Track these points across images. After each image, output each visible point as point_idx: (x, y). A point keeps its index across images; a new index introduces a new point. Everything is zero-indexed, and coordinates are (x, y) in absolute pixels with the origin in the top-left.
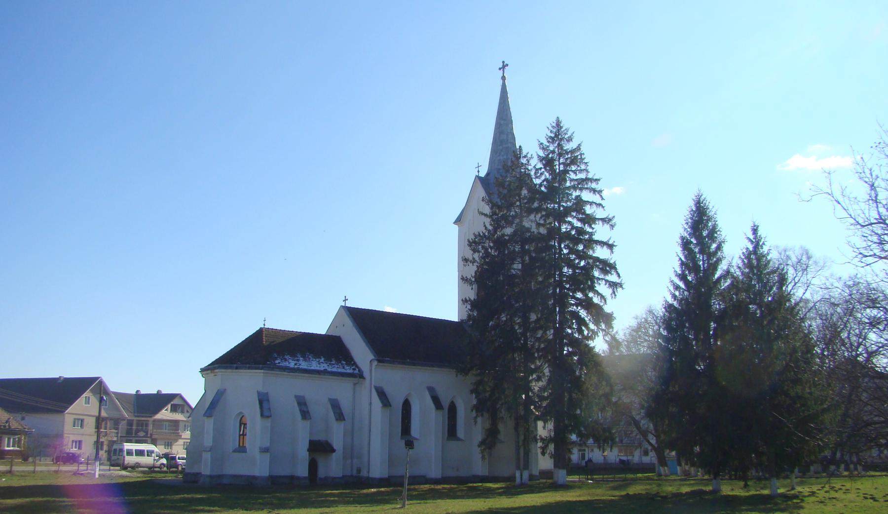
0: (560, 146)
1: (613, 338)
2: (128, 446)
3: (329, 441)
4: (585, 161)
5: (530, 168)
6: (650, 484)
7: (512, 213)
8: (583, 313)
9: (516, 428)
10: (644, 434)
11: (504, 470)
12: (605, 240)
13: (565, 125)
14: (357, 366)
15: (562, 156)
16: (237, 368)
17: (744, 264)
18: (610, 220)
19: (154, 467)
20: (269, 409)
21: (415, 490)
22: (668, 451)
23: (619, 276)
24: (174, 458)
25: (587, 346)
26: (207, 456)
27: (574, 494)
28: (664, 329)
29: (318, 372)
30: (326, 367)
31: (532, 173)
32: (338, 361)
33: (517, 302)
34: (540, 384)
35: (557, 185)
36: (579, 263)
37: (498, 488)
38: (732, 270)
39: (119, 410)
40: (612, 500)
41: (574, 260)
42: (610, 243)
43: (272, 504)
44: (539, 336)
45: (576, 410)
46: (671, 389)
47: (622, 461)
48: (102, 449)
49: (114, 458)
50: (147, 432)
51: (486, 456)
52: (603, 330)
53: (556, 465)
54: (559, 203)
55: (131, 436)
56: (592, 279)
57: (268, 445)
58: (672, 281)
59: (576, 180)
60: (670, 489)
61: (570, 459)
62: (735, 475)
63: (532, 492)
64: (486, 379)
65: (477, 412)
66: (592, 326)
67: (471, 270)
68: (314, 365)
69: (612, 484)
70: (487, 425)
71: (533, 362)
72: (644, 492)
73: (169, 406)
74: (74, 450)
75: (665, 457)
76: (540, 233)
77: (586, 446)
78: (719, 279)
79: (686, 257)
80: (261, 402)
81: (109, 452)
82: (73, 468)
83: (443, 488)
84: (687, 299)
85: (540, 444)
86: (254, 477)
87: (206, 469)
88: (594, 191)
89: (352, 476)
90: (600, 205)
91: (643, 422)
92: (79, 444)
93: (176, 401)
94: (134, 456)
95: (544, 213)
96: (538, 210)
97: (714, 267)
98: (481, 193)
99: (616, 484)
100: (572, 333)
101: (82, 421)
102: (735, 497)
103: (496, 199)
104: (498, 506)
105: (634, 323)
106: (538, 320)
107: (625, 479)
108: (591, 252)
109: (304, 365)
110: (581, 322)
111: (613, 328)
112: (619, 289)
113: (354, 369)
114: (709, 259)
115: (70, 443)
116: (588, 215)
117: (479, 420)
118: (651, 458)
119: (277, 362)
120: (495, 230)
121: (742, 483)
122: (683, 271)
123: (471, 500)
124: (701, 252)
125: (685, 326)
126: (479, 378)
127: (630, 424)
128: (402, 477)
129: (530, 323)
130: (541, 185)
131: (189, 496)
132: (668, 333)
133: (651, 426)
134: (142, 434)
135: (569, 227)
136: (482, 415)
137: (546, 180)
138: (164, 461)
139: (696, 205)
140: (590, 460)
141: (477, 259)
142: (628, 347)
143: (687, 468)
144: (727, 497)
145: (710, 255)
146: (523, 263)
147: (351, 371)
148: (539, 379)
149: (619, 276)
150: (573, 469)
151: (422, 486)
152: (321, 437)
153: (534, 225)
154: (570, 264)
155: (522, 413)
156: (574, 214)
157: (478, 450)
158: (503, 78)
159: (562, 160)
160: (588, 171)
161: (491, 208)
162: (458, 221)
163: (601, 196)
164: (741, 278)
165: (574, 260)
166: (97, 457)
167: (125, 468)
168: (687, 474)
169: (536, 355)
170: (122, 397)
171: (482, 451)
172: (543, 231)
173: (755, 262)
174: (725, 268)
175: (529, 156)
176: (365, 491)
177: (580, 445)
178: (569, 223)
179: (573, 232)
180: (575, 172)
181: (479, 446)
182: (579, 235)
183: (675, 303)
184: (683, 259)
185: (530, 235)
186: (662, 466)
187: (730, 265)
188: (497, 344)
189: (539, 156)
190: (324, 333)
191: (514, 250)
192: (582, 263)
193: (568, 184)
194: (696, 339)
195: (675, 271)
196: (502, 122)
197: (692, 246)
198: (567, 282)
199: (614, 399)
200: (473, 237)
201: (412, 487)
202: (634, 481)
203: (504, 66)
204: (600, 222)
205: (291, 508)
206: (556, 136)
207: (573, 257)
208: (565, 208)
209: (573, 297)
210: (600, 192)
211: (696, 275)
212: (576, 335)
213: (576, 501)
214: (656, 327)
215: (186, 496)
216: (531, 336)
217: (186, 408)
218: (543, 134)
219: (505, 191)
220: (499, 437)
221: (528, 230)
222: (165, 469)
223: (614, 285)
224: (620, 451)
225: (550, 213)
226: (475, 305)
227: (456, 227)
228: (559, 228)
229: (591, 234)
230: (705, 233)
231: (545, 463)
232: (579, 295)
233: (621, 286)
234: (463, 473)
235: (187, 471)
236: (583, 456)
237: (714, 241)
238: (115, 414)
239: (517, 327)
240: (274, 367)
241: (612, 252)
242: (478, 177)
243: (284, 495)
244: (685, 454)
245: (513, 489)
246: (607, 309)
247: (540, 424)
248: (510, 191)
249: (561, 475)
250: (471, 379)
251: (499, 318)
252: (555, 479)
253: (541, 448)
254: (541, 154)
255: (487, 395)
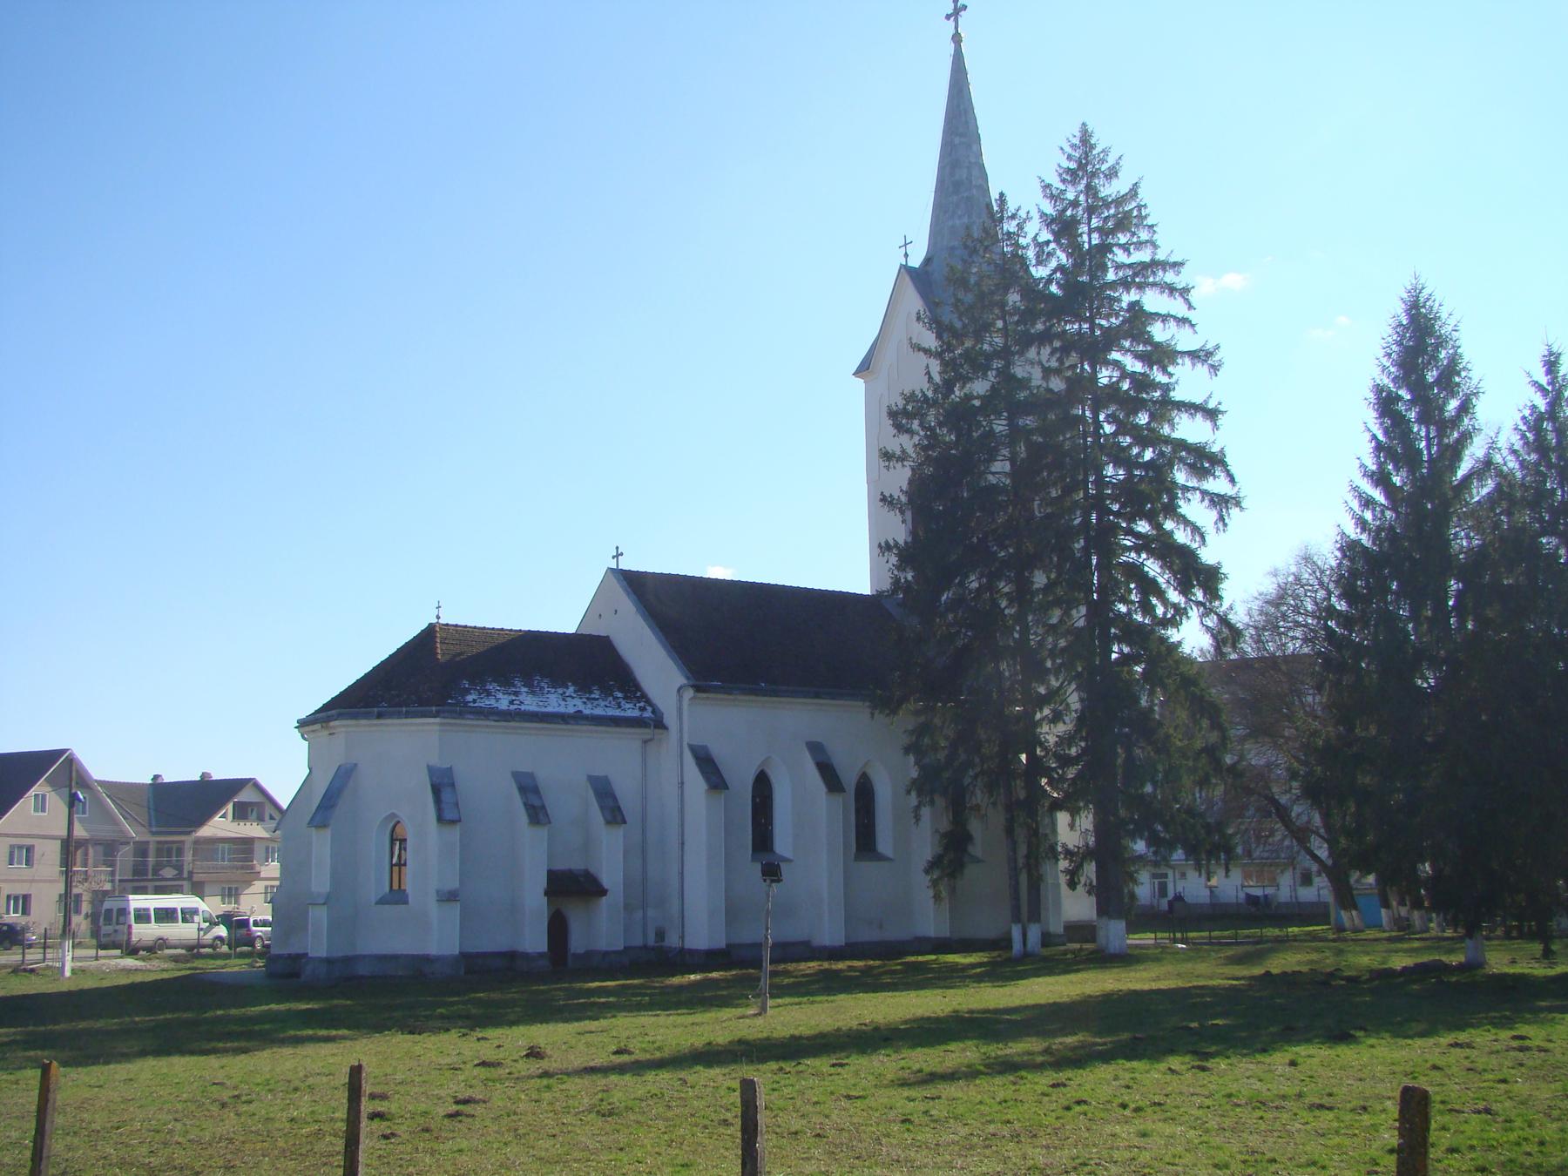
0: (1090, 190)
1: (1224, 620)
2: (137, 902)
3: (592, 870)
4: (1149, 221)
5: (1023, 241)
6: (1317, 950)
8: (1152, 567)
10: (1301, 835)
11: (988, 924)
12: (1198, 401)
13: (1100, 141)
14: (648, 702)
15: (1095, 210)
16: (380, 716)
17: (1527, 443)
18: (1209, 354)
20: (457, 805)
21: (786, 973)
23: (1232, 480)
24: (245, 924)
27: (1145, 974)
28: (1340, 597)
29: (563, 718)
30: (581, 707)
31: (1031, 254)
32: (607, 692)
34: (1061, 728)
35: (1085, 278)
36: (1140, 455)
37: (973, 966)
38: (1498, 459)
39: (115, 822)
40: (1233, 988)
42: (1211, 405)
43: (468, 1017)
44: (1054, 621)
45: (1142, 786)
48: (78, 912)
49: (106, 929)
50: (179, 868)
51: (944, 894)
52: (1199, 604)
53: (1102, 910)
54: (1091, 320)
56: (1171, 489)
57: (453, 883)
58: (1355, 489)
59: (1130, 266)
60: (1365, 960)
61: (1132, 896)
62: (1519, 928)
64: (937, 721)
66: (1174, 596)
67: (899, 479)
68: (554, 702)
69: (1230, 952)
70: (945, 825)
71: (1043, 681)
72: (1305, 969)
73: (230, 806)
76: (1051, 391)
78: (1467, 479)
79: (1386, 432)
80: (437, 790)
81: (94, 917)
83: (851, 968)
84: (1391, 528)
85: (1063, 864)
86: (427, 959)
87: (317, 944)
88: (1171, 289)
89: (645, 947)
90: (1183, 321)
91: (1297, 809)
92: (24, 903)
93: (245, 796)
94: (153, 925)
95: (1057, 344)
96: (1044, 338)
97: (1454, 453)
98: (914, 302)
99: (1240, 950)
100: (1129, 613)
101: (30, 849)
103: (948, 316)
104: (975, 1006)
105: (1270, 587)
108: (1166, 430)
109: (530, 703)
110: (1150, 587)
111: (1220, 598)
112: (1234, 511)
113: (642, 709)
114: (1441, 434)
116: (1157, 346)
117: (926, 812)
118: (1320, 890)
119: (470, 698)
121: (1537, 947)
122: (1380, 465)
123: (913, 994)
124: (1423, 419)
125: (1388, 590)
126: (922, 719)
127: (1269, 814)
128: (758, 946)
129: (1034, 593)
130: (1049, 281)
131: (282, 1007)
132: (1349, 604)
133: (1317, 819)
134: (169, 872)
135: (1116, 374)
136: (932, 803)
137: (1060, 268)
138: (222, 931)
139: (1408, 312)
140: (1179, 898)
141: (910, 451)
142: (1258, 640)
143: (1403, 911)
145: (1444, 425)
146: (1012, 460)
147: (636, 713)
148: (1056, 718)
149: (1232, 480)
150: (1143, 919)
151: (803, 966)
152: (575, 864)
153: (1037, 374)
154: (1121, 458)
155: (1022, 795)
156: (1127, 344)
157: (925, 880)
158: (957, 38)
159: (1095, 222)
160: (1155, 246)
161: (939, 336)
162: (864, 369)
163: (1187, 301)
164: (1519, 475)
165: (1130, 446)
166: (67, 930)
167: (132, 951)
168: (1404, 928)
169: (1049, 664)
170: (121, 791)
171: (935, 883)
172: (1057, 384)
173: (1552, 438)
174: (1480, 453)
175: (1022, 214)
177: (1156, 864)
178: (1117, 364)
179: (1125, 386)
180: (1125, 248)
181: (927, 872)
182: (1138, 391)
183: (1365, 539)
184: (1381, 437)
186: (1345, 908)
187: (1492, 446)
189: (1043, 215)
190: (567, 623)
192: (1148, 455)
193: (1111, 276)
194: (1415, 616)
195: (1362, 465)
196: (957, 140)
197: (1401, 407)
198: (1115, 499)
199: (1229, 760)
200: (901, 403)
201: (781, 967)
202: (1282, 943)
203: (957, 11)
204: (1187, 360)
205: (512, 1024)
206: (1081, 166)
208: (1107, 331)
209: (1130, 532)
210: (1184, 292)
211: (1412, 471)
212: (1138, 617)
213: (1151, 991)
214: (1321, 594)
215: (274, 1006)
216: (1037, 622)
217: (269, 810)
218: (1051, 163)
220: (970, 849)
221: (1024, 383)
222: (225, 949)
223: (1221, 503)
224: (1247, 876)
225: (1070, 345)
226: (907, 555)
227: (860, 383)
228: (1094, 378)
229: (1166, 388)
230: (1431, 376)
231: (1076, 906)
232: (1143, 527)
233: (1238, 504)
234: (893, 933)
235: (274, 951)
236: (1163, 890)
237: (1453, 394)
238: (105, 832)
239: (1004, 604)
241: (1216, 427)
243: (495, 996)
246: (1207, 556)
247: (1063, 818)
249: (1115, 934)
250: (906, 719)
251: (961, 584)
253: (1067, 871)
254: (1049, 209)
255: (942, 755)
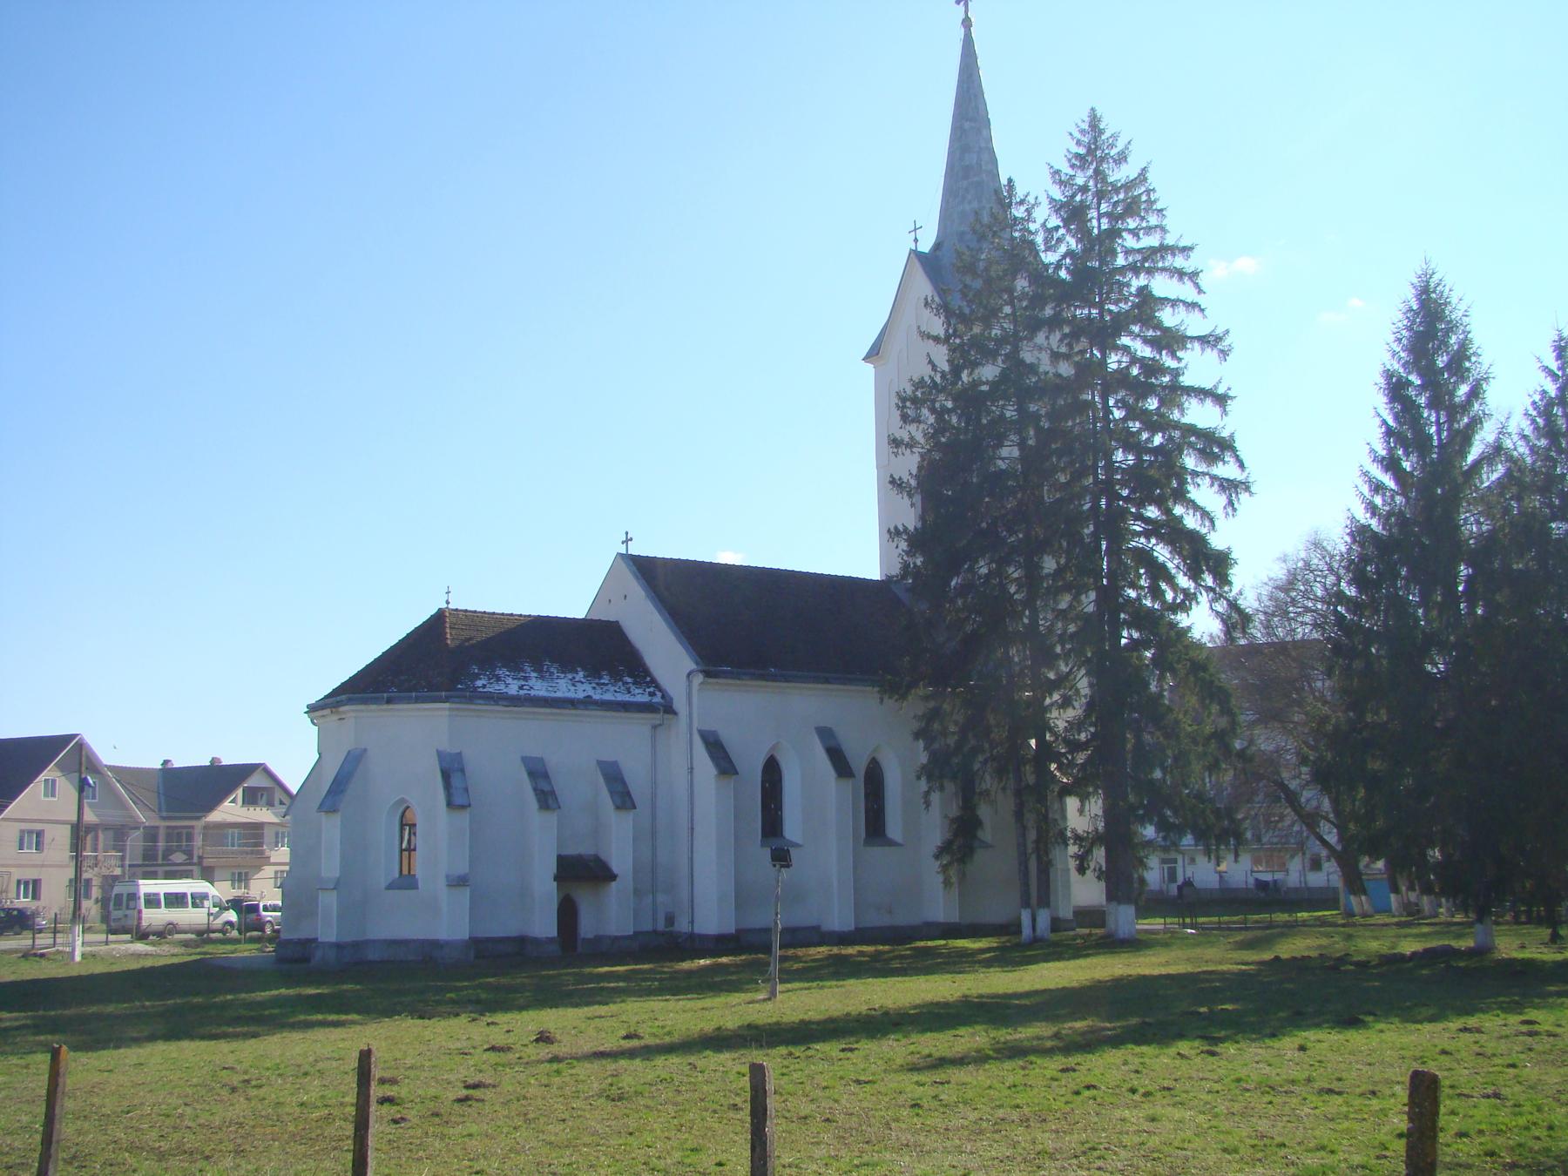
1: (1233, 605)
2: (147, 886)
3: (603, 856)
5: (1032, 227)
7: (996, 332)
8: (1162, 553)
9: (1019, 815)
10: (1310, 820)
11: (996, 908)
12: (1208, 385)
13: (1109, 125)
14: (658, 687)
15: (1105, 196)
16: (389, 701)
17: (1537, 428)
18: (1219, 339)
19: (210, 930)
20: (466, 790)
21: (796, 958)
22: (1366, 859)
23: (1242, 466)
25: (1173, 625)
26: (329, 900)
28: (1349, 583)
30: (591, 693)
31: (1039, 239)
32: (616, 677)
33: (1012, 532)
34: (1070, 714)
36: (1149, 440)
38: (1508, 443)
39: (125, 807)
40: (1242, 973)
41: (1139, 432)
42: (1221, 391)
43: (478, 1002)
44: (1063, 605)
45: (1151, 772)
46: (1369, 718)
47: (1262, 885)
48: (88, 896)
49: (116, 914)
50: (189, 853)
52: (1209, 589)
54: (1100, 306)
55: (152, 865)
56: (1181, 474)
58: (1365, 474)
59: (1139, 251)
60: (1374, 945)
61: (1142, 881)
62: (1529, 913)
63: (1059, 957)
65: (929, 779)
66: (1183, 581)
67: (908, 464)
68: (564, 687)
69: (1239, 937)
70: (954, 811)
71: (1051, 667)
72: (1314, 954)
73: (240, 792)
74: (24, 902)
75: (1360, 874)
76: (1059, 376)
77: (1177, 851)
78: (1477, 464)
79: (1396, 417)
80: (446, 776)
81: (104, 902)
82: (22, 941)
83: (861, 953)
85: (1073, 849)
86: (436, 944)
87: (327, 930)
88: (1180, 274)
89: (655, 932)
90: (1193, 306)
91: (1306, 794)
92: (34, 888)
93: (255, 781)
95: (1067, 330)
96: (1055, 323)
98: (923, 287)
99: (1250, 935)
100: (1139, 598)
101: (40, 834)
102: (1529, 963)
103: (956, 302)
104: (984, 990)
105: (1279, 573)
106: (1059, 572)
107: (1271, 925)
108: (1176, 415)
109: (539, 688)
110: (1159, 572)
111: (1230, 583)
112: (1244, 496)
113: (652, 694)
114: (1451, 419)
115: (14, 886)
116: (1166, 330)
117: (935, 797)
118: (1329, 875)
119: (479, 683)
120: (956, 371)
121: (1546, 933)
122: (1390, 450)
123: (922, 978)
124: (1434, 404)
126: (932, 704)
128: (767, 931)
130: (1058, 266)
131: (291, 992)
133: (1326, 804)
134: (179, 857)
136: (942, 788)
137: (1069, 254)
138: (232, 916)
139: (1418, 297)
140: (1188, 883)
141: (919, 437)
142: (1268, 626)
143: (1413, 896)
144: (1512, 962)
145: (1454, 410)
146: (1022, 445)
147: (645, 698)
148: (1066, 703)
149: (1242, 466)
150: (1154, 904)
153: (1045, 358)
156: (1136, 329)
158: (967, 23)
159: (1104, 207)
160: (1163, 229)
162: (873, 354)
163: (1197, 285)
164: (1529, 460)
165: (1139, 432)
166: (77, 915)
167: (142, 936)
168: (1413, 911)
169: (1058, 649)
170: (131, 777)
171: (945, 868)
172: (1066, 369)
174: (1491, 438)
175: (1031, 199)
176: (686, 965)
177: (1165, 849)
178: (1126, 349)
179: (1135, 371)
180: (1134, 233)
181: (937, 857)
183: (1374, 524)
184: (1391, 422)
185: (1035, 381)
187: (1502, 431)
188: (969, 628)
189: (1052, 200)
191: (1002, 415)
192: (1158, 440)
193: (1120, 261)
194: (1425, 601)
195: (1372, 451)
196: (967, 125)
197: (1411, 392)
198: (1124, 484)
199: (1238, 745)
201: (791, 952)
202: (1291, 928)
204: (1197, 345)
205: (521, 1008)
206: (1090, 151)
207: (1135, 426)
208: (1116, 317)
209: (1139, 517)
210: (1193, 276)
212: (1148, 603)
213: (1161, 976)
214: (1331, 579)
215: (283, 991)
217: (278, 795)
218: (1059, 149)
219: (978, 284)
220: (980, 834)
221: (1032, 369)
222: (235, 934)
223: (1230, 488)
224: (1257, 861)
225: (1081, 329)
226: (918, 541)
227: (869, 368)
228: (1103, 363)
229: (1176, 373)
230: (1441, 361)
231: (1086, 891)
232: (1152, 512)
234: (902, 918)
235: (284, 936)
237: (1463, 380)
238: (115, 816)
239: (1013, 589)
240: (474, 696)
241: (1225, 412)
242: (915, 254)
243: (504, 980)
244: (1405, 864)
245: (1018, 949)
246: (1217, 541)
247: (1072, 803)
248: (989, 281)
249: (1125, 919)
252: (1111, 924)
253: (1076, 856)
255: (951, 741)
